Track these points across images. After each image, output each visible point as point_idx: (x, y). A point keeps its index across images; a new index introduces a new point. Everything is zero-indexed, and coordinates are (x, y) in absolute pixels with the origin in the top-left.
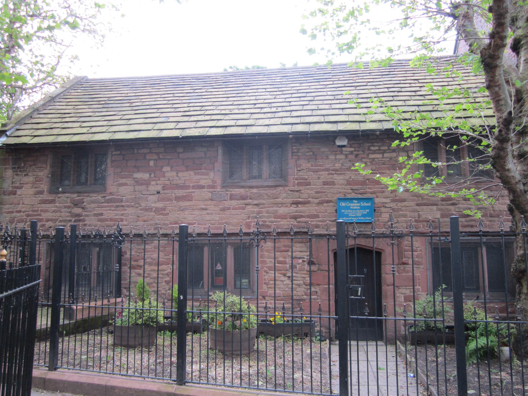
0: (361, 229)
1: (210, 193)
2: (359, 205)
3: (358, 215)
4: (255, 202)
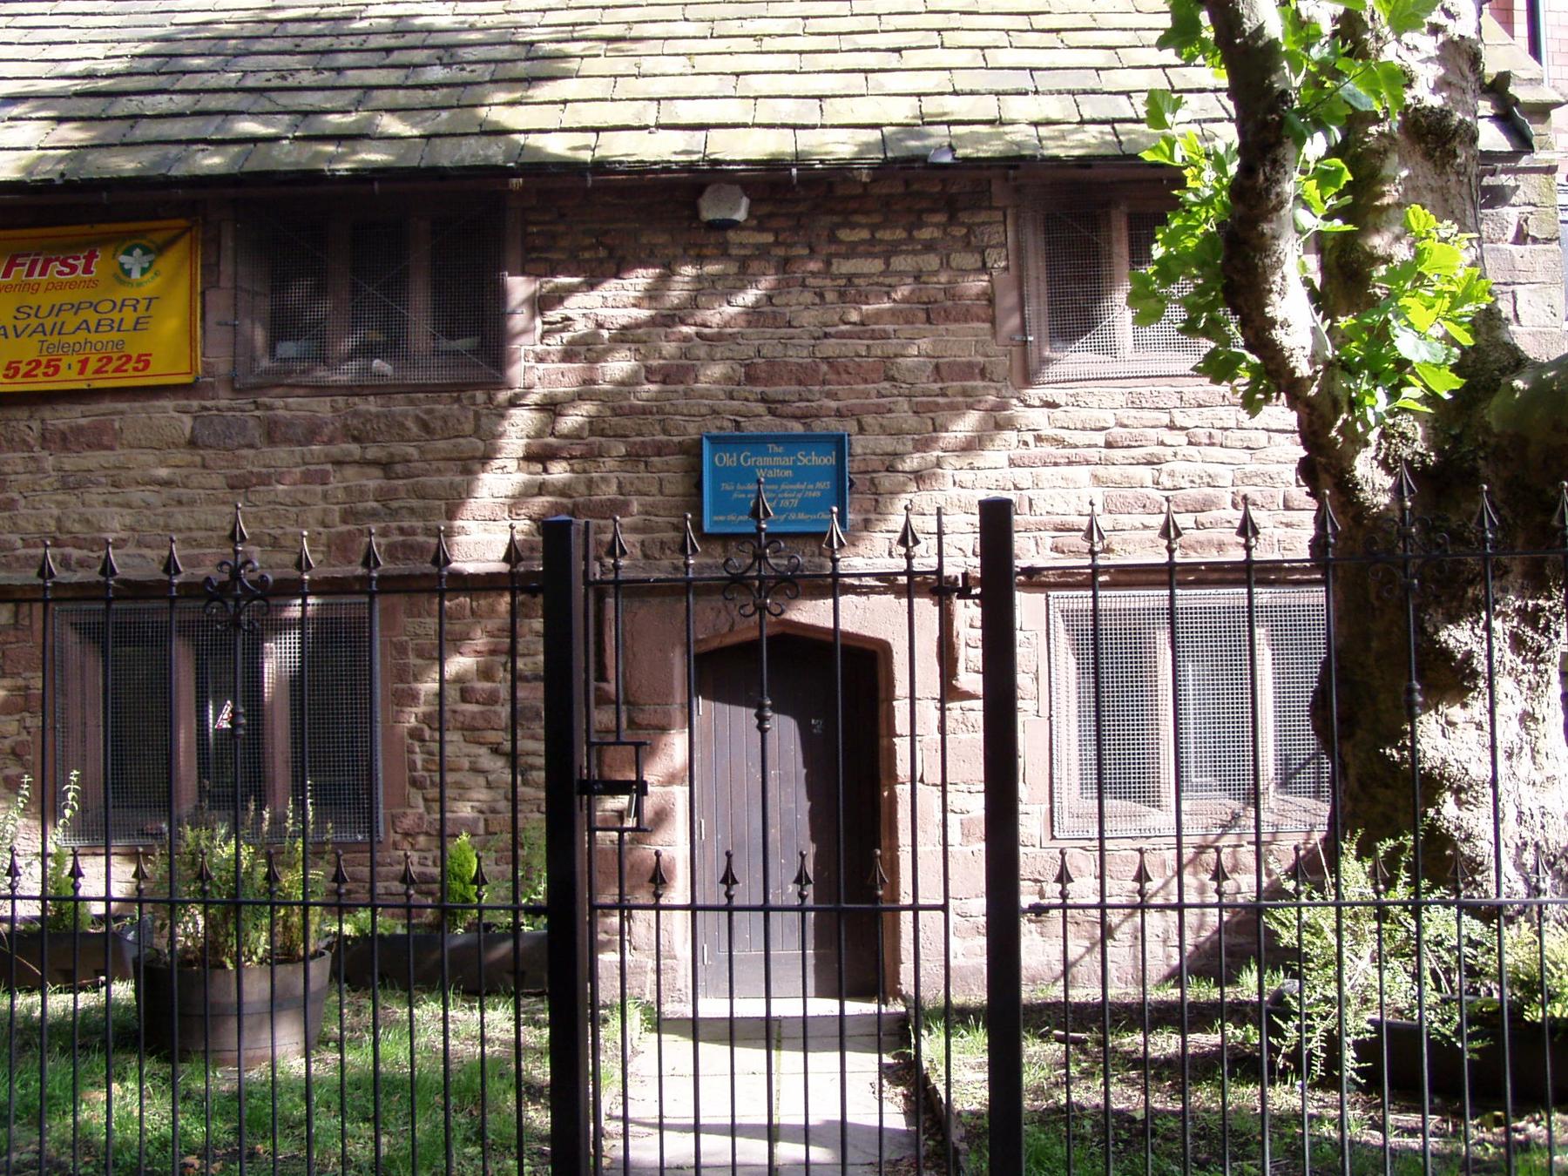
2: (788, 461)
4: (373, 452)
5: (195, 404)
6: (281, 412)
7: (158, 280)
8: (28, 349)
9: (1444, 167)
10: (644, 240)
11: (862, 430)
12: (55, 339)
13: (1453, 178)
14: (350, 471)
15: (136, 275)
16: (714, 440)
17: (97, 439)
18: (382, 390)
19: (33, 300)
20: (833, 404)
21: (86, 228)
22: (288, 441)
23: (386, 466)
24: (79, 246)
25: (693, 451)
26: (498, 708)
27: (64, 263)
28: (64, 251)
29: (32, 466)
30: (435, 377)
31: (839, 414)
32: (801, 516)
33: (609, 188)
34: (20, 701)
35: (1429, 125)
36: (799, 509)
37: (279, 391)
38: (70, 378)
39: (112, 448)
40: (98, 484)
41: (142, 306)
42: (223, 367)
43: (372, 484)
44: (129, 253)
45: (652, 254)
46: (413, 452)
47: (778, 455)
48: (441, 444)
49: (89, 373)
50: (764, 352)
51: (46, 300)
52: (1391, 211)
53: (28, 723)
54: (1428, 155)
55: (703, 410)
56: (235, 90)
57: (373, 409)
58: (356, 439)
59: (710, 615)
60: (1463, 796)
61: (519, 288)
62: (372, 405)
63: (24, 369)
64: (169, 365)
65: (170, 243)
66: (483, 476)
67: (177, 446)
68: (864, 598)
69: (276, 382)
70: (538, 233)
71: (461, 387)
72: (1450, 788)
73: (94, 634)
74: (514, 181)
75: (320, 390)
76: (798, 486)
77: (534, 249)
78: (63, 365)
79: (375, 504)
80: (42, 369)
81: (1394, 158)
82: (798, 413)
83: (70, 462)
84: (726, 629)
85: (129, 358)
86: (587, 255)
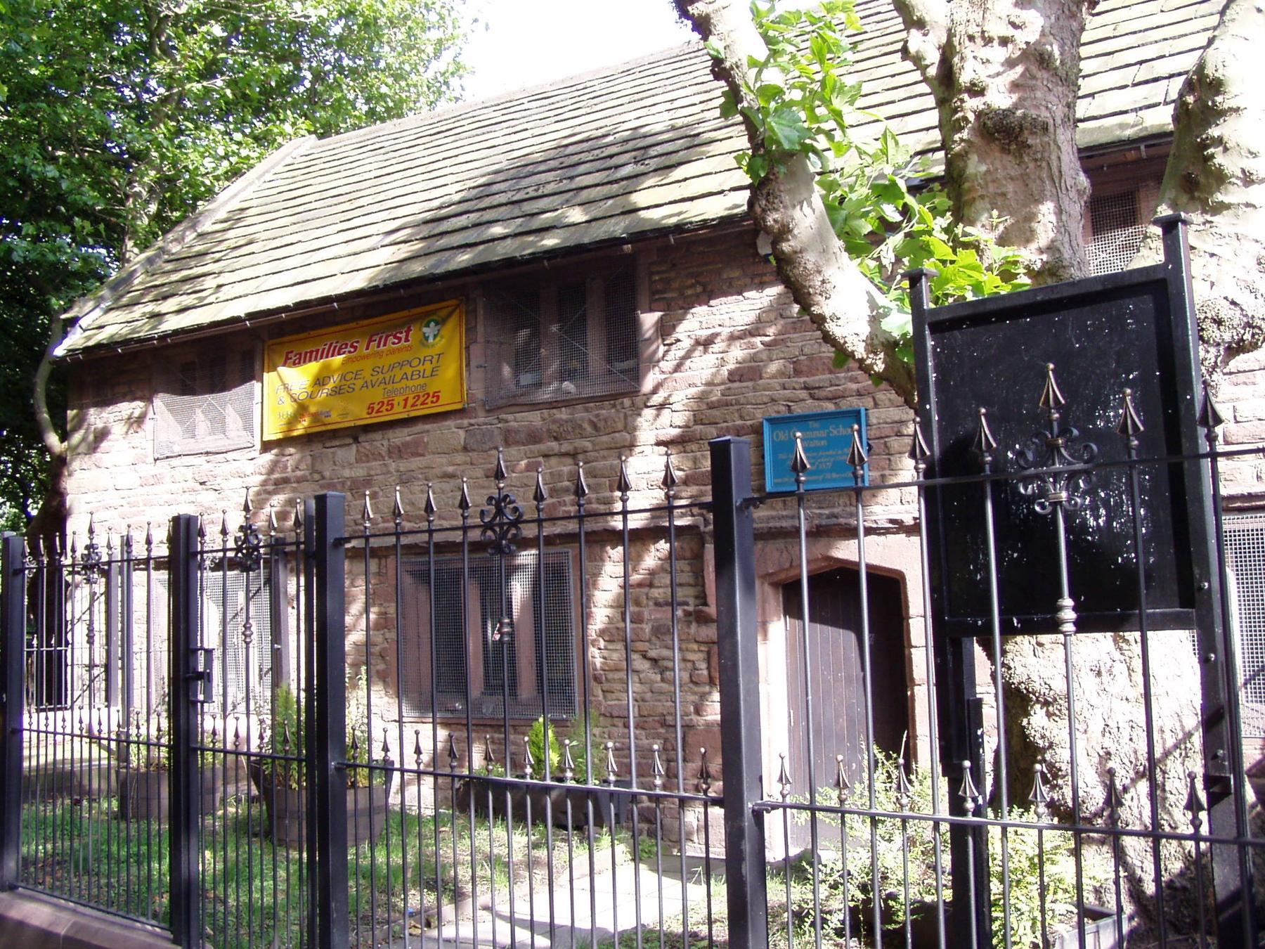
0: (836, 510)
1: (462, 432)
2: (823, 433)
3: (822, 466)
4: (566, 447)
5: (466, 422)
6: (512, 424)
7: (444, 341)
8: (377, 395)
9: (1021, 156)
10: (725, 276)
11: (876, 405)
12: (390, 387)
13: (1031, 165)
14: (553, 461)
15: (431, 340)
16: (771, 421)
17: (412, 450)
18: (568, 403)
19: (380, 362)
20: (854, 386)
21: (406, 313)
22: (517, 443)
23: (573, 455)
24: (404, 324)
25: (758, 431)
26: (644, 626)
27: (395, 337)
28: (393, 329)
29: (384, 469)
30: (599, 391)
31: (859, 394)
32: (834, 475)
33: (690, 244)
34: (382, 621)
35: (995, 125)
36: (831, 471)
37: (512, 409)
38: (399, 413)
39: (423, 455)
40: (418, 479)
41: (434, 360)
42: (479, 394)
43: (566, 469)
44: (427, 326)
45: (730, 285)
46: (588, 445)
47: (816, 429)
48: (605, 439)
49: (408, 408)
50: (806, 350)
51: (386, 361)
52: (977, 203)
53: (388, 635)
54: (1005, 150)
55: (765, 400)
56: (506, 204)
57: (564, 416)
58: (556, 439)
59: (777, 554)
60: (1051, 709)
61: (649, 320)
62: (563, 414)
63: (376, 407)
64: (449, 401)
65: (449, 315)
66: (630, 459)
67: (457, 451)
68: (883, 537)
69: (516, 403)
70: (661, 280)
71: (615, 397)
72: (1038, 701)
73: (422, 576)
74: (625, 247)
75: (535, 406)
76: (831, 452)
77: (657, 292)
78: (395, 403)
79: (567, 483)
80: (385, 407)
81: (974, 158)
82: (830, 395)
83: (403, 465)
84: (787, 565)
85: (428, 395)
86: (689, 292)
